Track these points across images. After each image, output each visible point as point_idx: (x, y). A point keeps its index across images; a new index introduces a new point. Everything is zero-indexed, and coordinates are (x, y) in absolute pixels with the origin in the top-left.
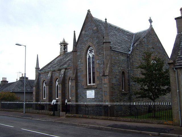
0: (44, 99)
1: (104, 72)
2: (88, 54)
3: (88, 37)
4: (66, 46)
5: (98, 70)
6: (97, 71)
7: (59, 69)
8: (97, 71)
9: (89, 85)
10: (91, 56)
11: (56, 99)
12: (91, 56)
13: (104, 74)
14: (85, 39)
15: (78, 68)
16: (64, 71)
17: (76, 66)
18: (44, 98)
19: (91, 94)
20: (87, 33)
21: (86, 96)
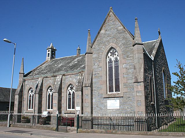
0: (30, 110)
1: (136, 78)
2: (109, 57)
3: (110, 38)
4: (54, 52)
5: (125, 76)
6: (124, 77)
7: (54, 76)
8: (124, 77)
9: (111, 93)
10: (113, 59)
11: (47, 110)
12: (113, 59)
13: (137, 80)
14: (104, 39)
15: (93, 73)
16: (61, 77)
17: (91, 70)
18: (30, 108)
19: (113, 104)
20: (107, 32)
21: (106, 106)
